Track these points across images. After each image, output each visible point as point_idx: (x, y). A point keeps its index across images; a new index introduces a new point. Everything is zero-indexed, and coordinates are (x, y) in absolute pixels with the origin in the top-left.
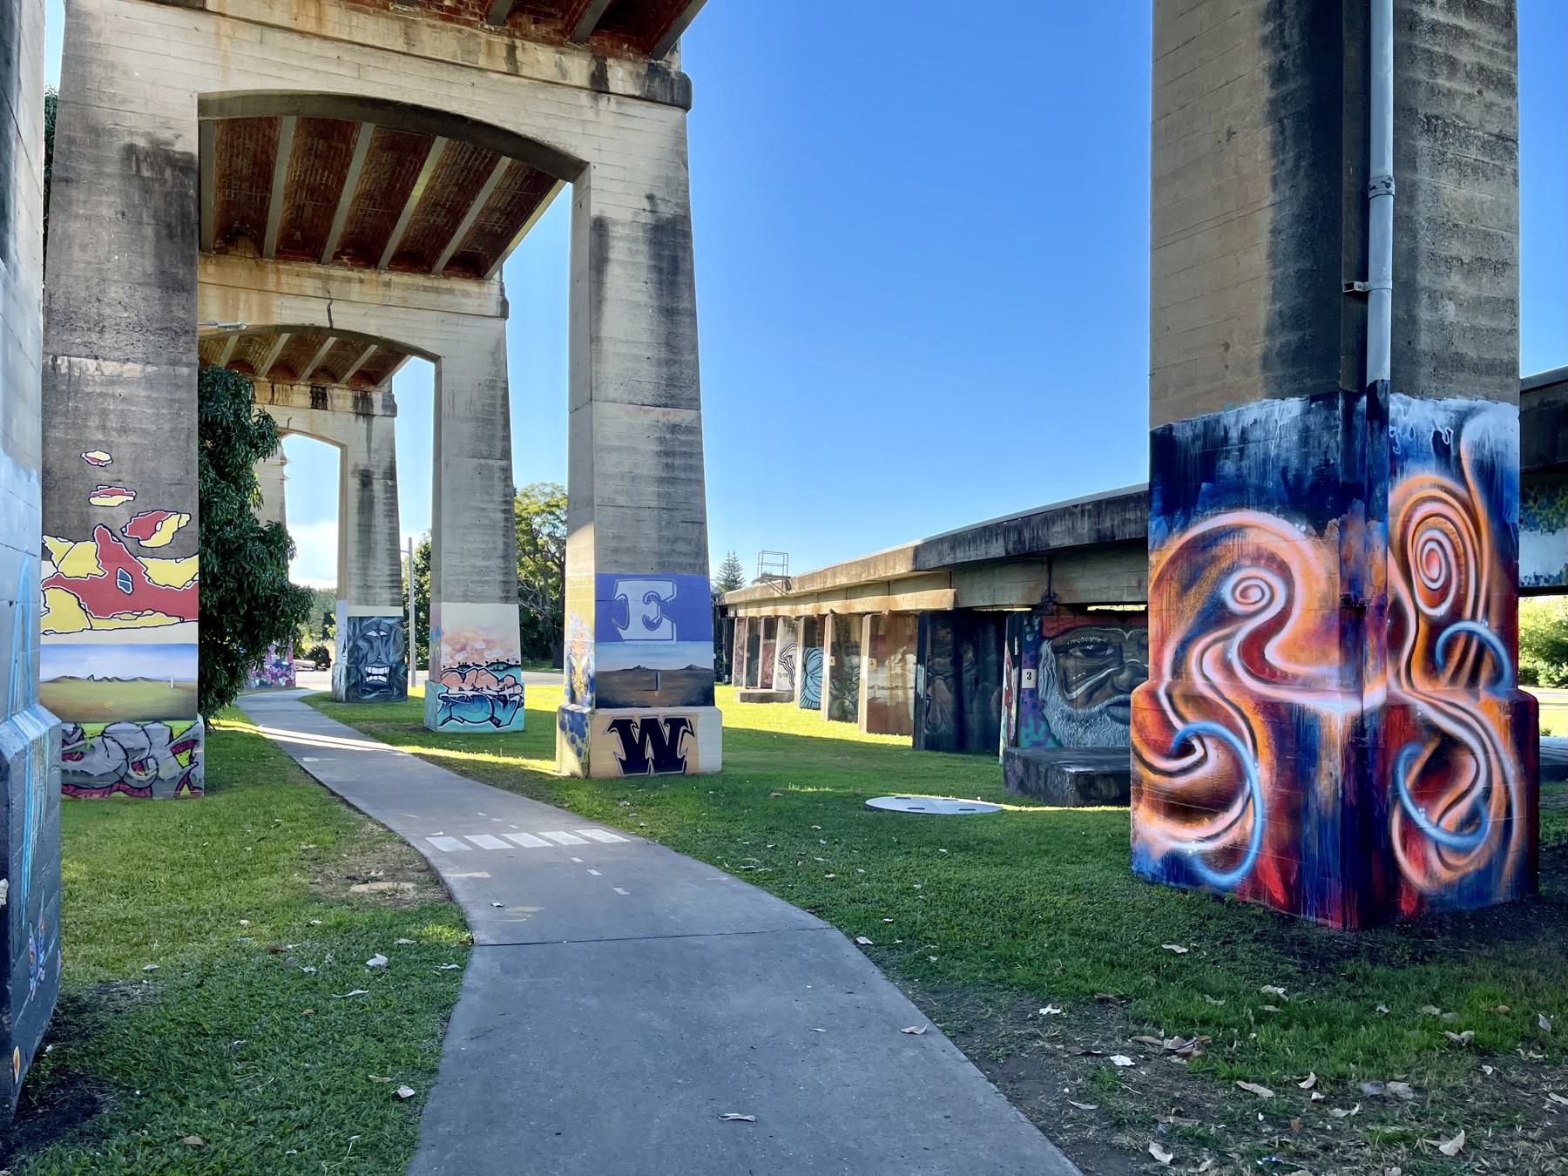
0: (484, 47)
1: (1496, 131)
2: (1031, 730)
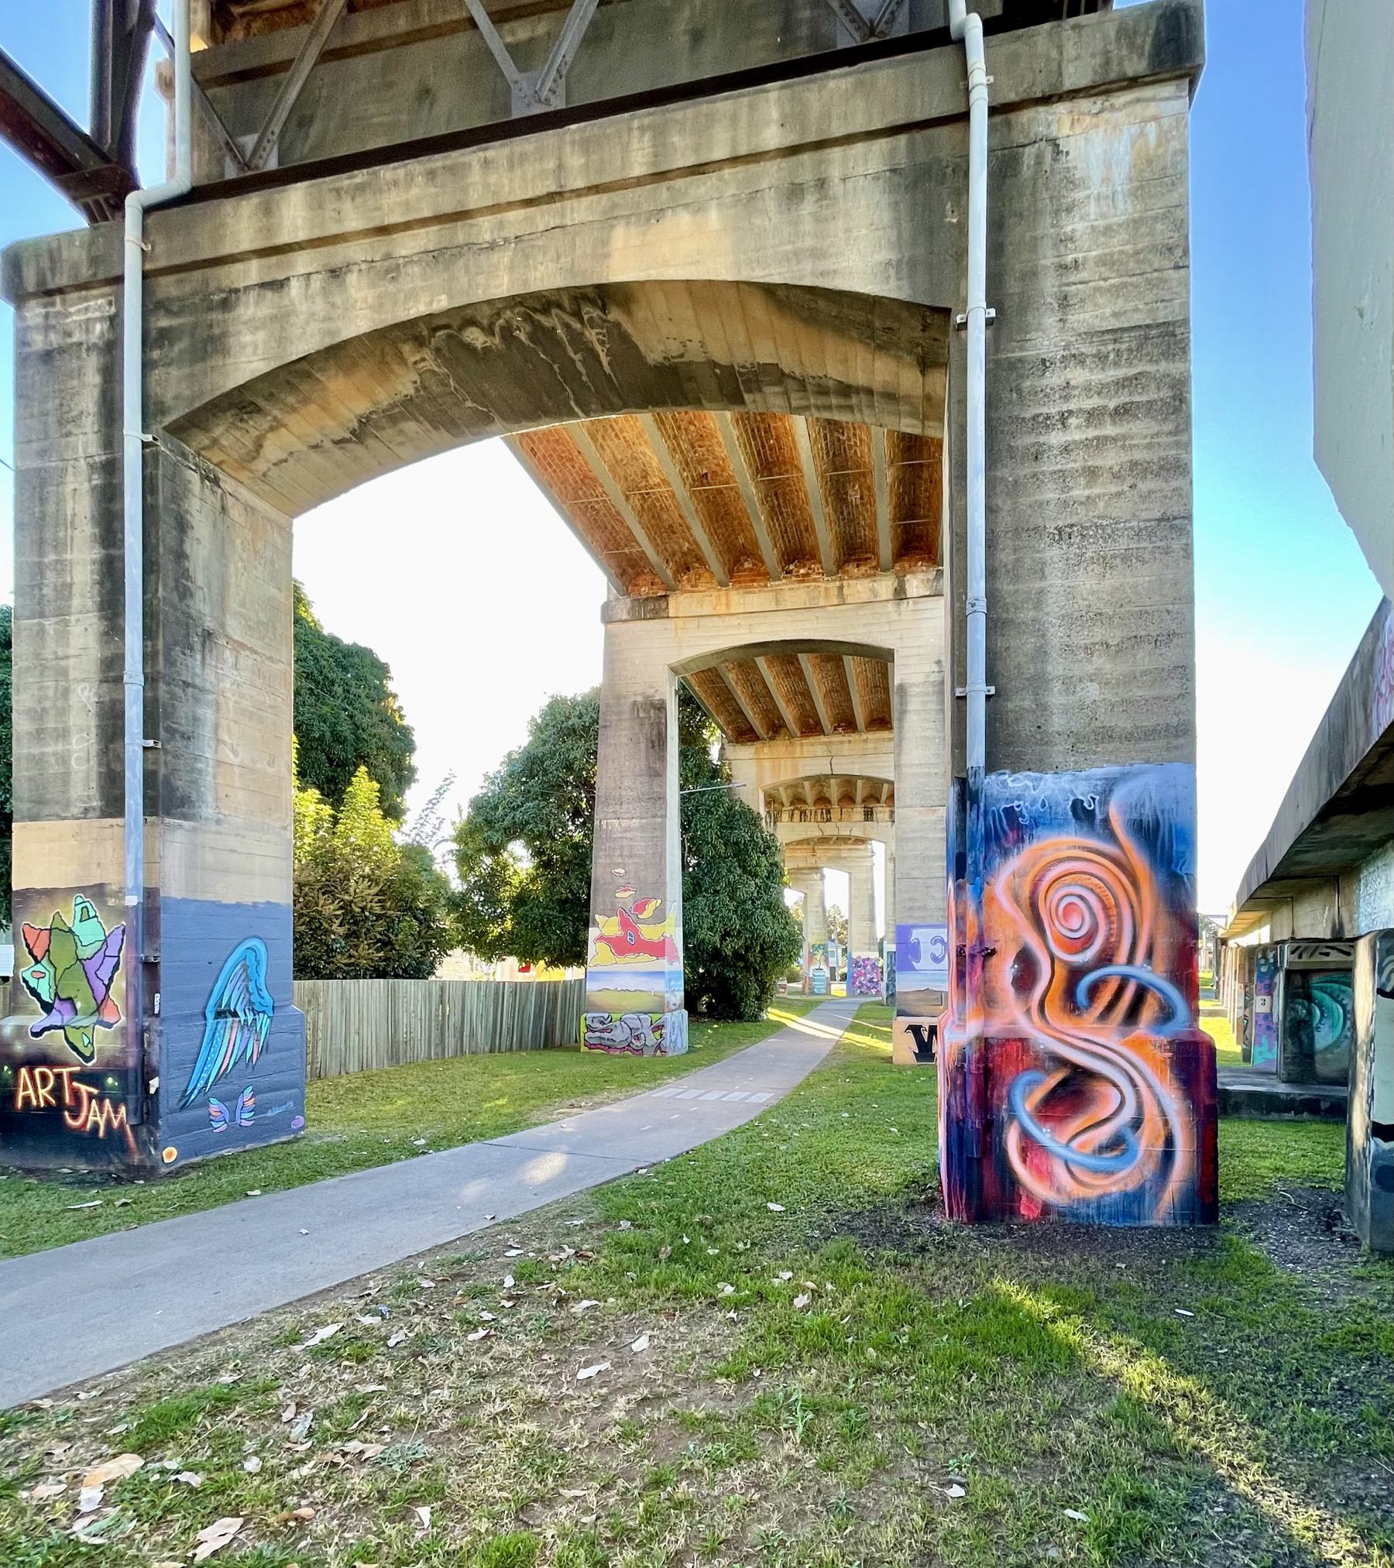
0: (823, 593)
1: (1158, 515)
2: (1265, 1048)
